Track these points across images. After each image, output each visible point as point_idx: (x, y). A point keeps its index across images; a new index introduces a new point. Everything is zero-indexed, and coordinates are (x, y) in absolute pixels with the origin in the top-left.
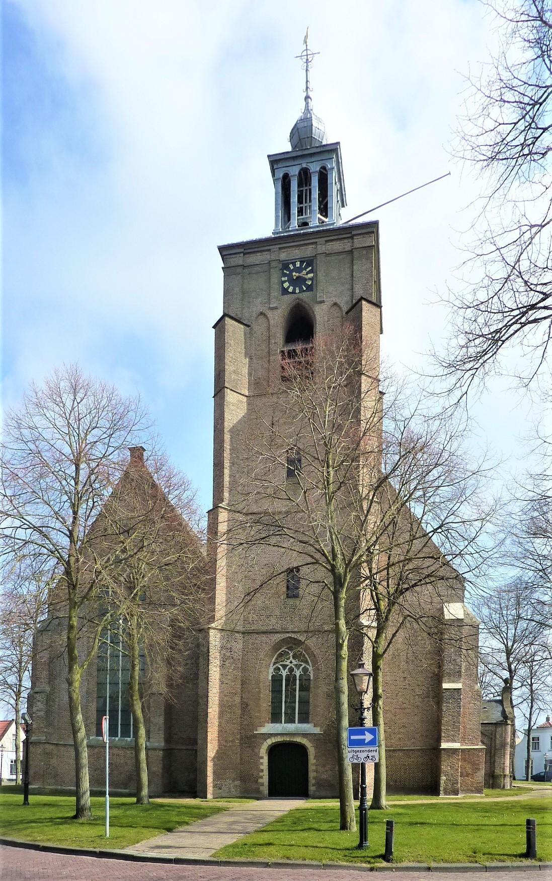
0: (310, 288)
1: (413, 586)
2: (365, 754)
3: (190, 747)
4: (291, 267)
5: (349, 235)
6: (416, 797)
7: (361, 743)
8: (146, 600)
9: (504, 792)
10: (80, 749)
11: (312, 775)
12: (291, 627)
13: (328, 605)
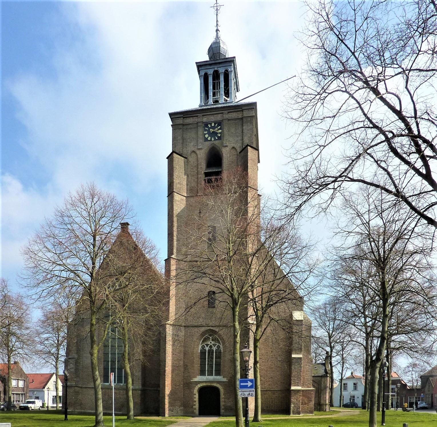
0: (220, 138)
1: (275, 303)
2: (248, 393)
3: (156, 389)
4: (209, 126)
5: (241, 110)
6: (277, 415)
7: (246, 387)
8: (134, 311)
9: (325, 413)
10: (98, 390)
11: (222, 404)
12: (211, 324)
13: (229, 313)
